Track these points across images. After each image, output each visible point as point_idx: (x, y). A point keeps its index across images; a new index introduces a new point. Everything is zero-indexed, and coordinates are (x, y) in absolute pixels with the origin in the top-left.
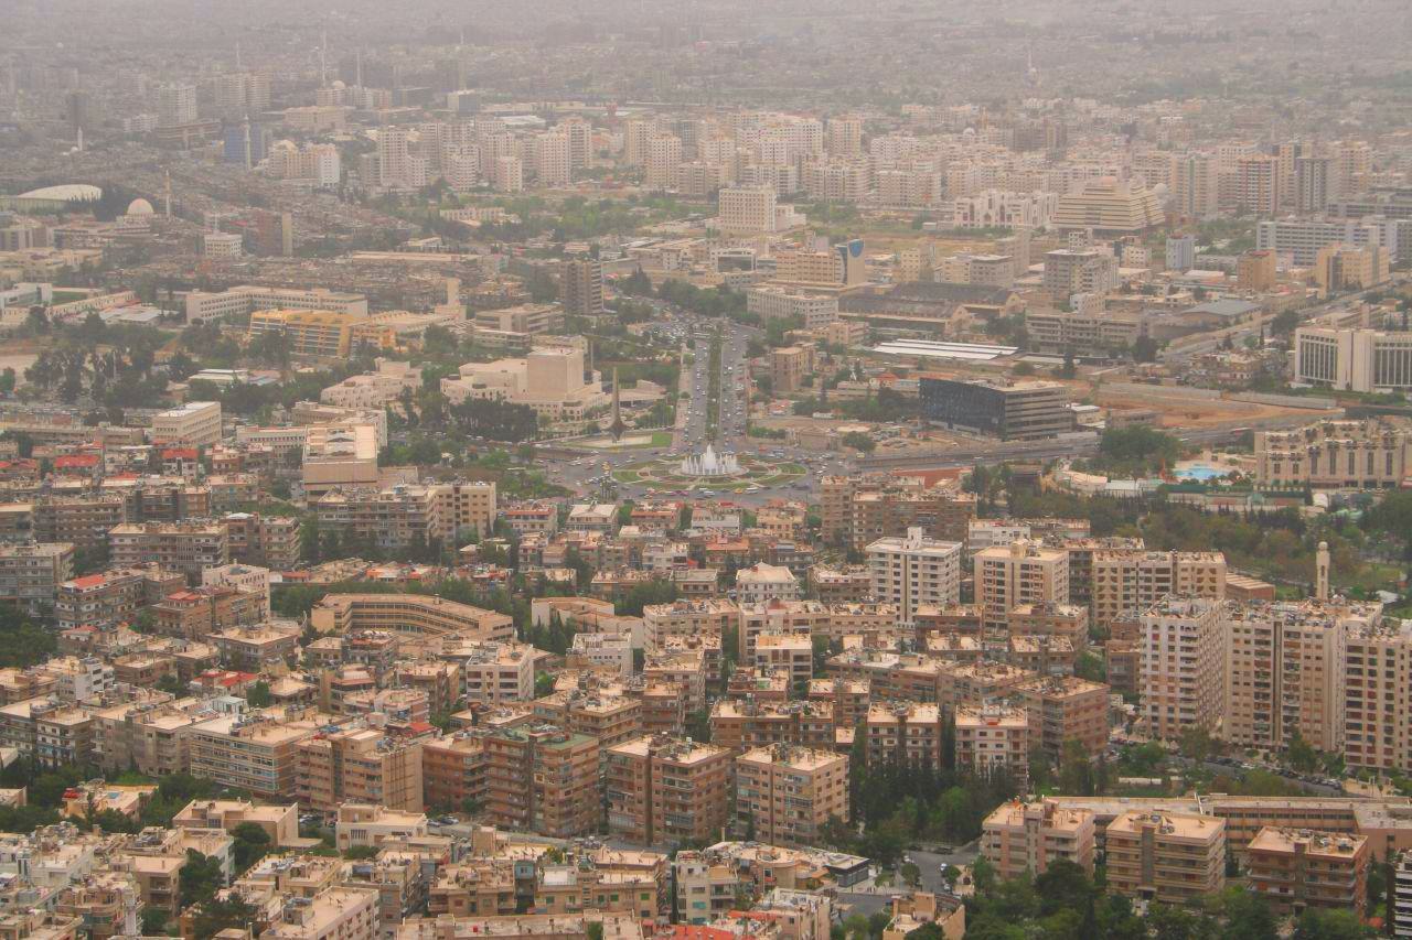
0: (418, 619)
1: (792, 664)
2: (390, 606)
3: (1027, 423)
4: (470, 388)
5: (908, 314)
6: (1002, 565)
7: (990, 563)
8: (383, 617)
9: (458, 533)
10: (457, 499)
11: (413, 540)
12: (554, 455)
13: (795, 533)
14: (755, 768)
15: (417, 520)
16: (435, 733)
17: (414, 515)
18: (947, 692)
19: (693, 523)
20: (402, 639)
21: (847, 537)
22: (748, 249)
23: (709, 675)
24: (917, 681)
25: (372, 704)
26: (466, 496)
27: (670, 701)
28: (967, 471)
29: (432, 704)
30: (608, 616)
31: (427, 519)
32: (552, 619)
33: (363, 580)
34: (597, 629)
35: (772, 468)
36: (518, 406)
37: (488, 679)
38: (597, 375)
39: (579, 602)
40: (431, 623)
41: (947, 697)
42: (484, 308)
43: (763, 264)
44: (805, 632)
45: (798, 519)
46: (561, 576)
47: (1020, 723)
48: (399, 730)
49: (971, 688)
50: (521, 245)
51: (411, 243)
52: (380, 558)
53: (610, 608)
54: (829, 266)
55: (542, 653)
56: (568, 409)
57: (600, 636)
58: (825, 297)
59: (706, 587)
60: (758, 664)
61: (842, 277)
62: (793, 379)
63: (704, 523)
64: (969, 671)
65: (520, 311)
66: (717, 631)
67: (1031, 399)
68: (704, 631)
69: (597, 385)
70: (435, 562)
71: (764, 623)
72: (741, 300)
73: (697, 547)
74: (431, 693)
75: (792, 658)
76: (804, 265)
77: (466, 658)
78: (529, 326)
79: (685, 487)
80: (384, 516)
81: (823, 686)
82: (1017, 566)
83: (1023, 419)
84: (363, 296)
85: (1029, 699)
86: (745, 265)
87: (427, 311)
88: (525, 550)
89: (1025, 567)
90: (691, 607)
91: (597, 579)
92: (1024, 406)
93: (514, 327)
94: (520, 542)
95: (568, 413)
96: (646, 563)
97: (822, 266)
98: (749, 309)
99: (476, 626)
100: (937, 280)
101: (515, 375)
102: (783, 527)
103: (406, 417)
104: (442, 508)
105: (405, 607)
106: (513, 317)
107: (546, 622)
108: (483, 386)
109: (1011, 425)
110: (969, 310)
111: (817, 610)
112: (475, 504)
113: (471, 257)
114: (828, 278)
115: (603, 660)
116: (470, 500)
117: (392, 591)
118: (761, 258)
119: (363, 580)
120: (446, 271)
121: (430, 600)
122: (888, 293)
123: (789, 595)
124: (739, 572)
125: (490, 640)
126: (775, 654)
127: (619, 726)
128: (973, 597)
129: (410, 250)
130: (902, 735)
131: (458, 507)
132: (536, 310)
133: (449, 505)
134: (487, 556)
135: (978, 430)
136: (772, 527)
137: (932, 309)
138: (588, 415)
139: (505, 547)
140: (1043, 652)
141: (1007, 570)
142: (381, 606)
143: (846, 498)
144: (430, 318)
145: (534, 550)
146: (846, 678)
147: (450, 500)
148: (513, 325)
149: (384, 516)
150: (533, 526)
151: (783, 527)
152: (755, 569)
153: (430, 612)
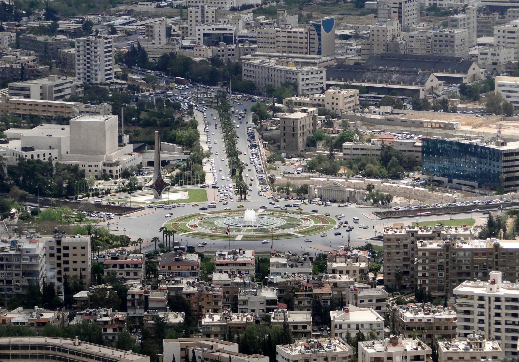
2: (33, 347)
4: (19, 150)
5: (387, 83)
26: (66, 248)
28: (482, 220)
35: (306, 219)
43: (243, 39)
45: (363, 265)
50: (17, 23)
53: (234, 347)
54: (304, 40)
56: (108, 169)
58: (314, 68)
59: (304, 327)
62: (300, 140)
65: (45, 81)
72: (237, 70)
76: (281, 44)
78: (55, 95)
79: (234, 237)
82: (493, 299)
88: (133, 295)
90: (320, 346)
91: (206, 320)
93: (43, 96)
95: (108, 172)
97: (299, 40)
98: (244, 78)
100: (402, 52)
101: (59, 139)
106: (41, 88)
108: (32, 149)
110: (439, 78)
112: (75, 255)
114: (298, 50)
116: (70, 251)
131: (59, 258)
132: (60, 81)
135: (476, 184)
137: (407, 78)
142: (25, 347)
143: (405, 246)
145: (140, 295)
148: (41, 94)
150: (128, 274)
153: (72, 353)
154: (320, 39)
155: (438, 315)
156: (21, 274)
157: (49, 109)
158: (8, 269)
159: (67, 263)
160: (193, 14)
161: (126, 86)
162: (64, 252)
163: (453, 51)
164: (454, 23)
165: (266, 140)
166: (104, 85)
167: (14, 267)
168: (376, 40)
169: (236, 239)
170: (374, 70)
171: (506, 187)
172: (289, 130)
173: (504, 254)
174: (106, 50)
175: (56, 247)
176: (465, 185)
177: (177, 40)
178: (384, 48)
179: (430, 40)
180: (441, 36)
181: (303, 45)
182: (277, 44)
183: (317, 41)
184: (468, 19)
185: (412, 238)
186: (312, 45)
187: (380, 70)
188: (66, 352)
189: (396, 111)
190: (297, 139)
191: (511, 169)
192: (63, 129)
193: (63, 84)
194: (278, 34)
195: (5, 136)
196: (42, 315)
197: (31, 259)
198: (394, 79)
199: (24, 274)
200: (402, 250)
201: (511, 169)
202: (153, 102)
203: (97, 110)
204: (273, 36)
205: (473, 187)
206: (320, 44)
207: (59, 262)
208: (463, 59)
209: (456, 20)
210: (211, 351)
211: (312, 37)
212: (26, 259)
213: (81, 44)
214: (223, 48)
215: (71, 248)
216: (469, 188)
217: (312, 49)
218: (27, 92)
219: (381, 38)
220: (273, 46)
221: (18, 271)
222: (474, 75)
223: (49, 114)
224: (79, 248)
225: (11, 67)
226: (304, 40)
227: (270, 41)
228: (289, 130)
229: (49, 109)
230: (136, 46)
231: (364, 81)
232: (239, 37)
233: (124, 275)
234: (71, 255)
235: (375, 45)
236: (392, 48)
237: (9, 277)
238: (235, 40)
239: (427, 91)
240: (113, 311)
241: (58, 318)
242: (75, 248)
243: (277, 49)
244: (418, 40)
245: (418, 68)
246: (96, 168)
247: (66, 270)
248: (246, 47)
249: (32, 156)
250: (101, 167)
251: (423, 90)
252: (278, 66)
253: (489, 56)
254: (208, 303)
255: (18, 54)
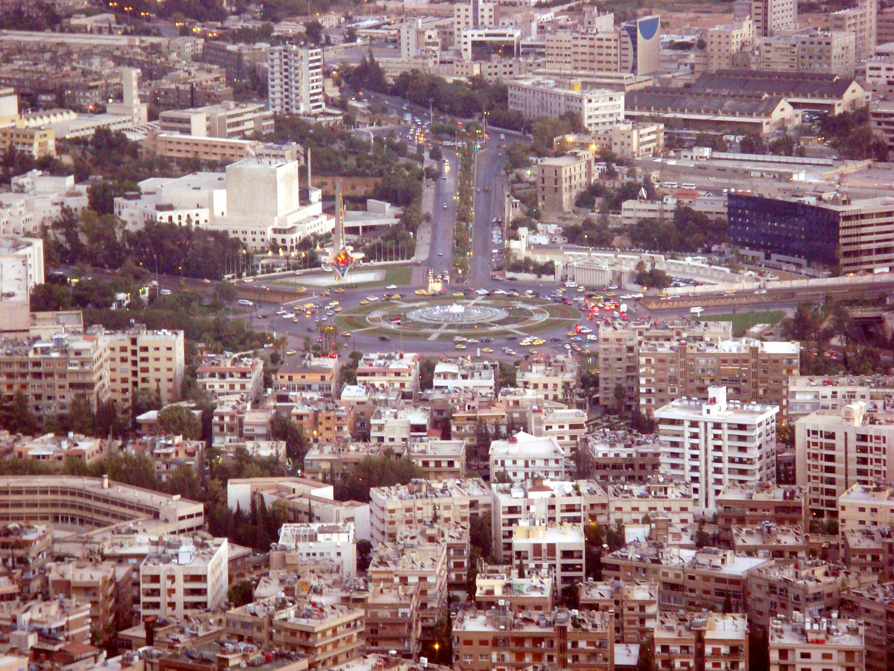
0: (81, 508)
1: (559, 561)
2: (44, 491)
3: (869, 252)
6: (832, 436)
7: (815, 433)
8: (35, 505)
9: (134, 398)
10: (134, 353)
11: (75, 404)
12: (261, 296)
13: (565, 394)
14: (69, 95)
15: (80, 379)
16: (96, 658)
17: (77, 373)
18: (760, 600)
19: (437, 382)
20: (59, 534)
21: (631, 399)
22: (509, 31)
23: (453, 576)
24: (722, 586)
25: (14, 620)
26: (145, 349)
27: (401, 610)
29: (94, 618)
30: (325, 501)
31: (95, 378)
32: (253, 503)
33: (8, 458)
34: (311, 517)
36: (215, 234)
37: (169, 585)
38: (316, 195)
39: (286, 482)
40: (98, 512)
41: (759, 607)
42: (168, 107)
44: (576, 520)
46: (265, 450)
47: (854, 643)
48: (49, 654)
49: (791, 596)
50: (219, 24)
51: (74, 21)
52: (33, 430)
53: (328, 492)
54: (613, 51)
55: (240, 550)
56: (279, 237)
57: (315, 526)
59: (451, 464)
60: (516, 562)
61: (630, 65)
62: (566, 197)
63: (450, 383)
64: (788, 573)
65: (218, 111)
66: (464, 519)
67: (875, 220)
68: (447, 520)
69: (316, 207)
70: (103, 435)
71: (524, 509)
73: (440, 412)
74: (94, 604)
75: (558, 554)
76: (580, 57)
77: (141, 557)
78: (229, 130)
80: (38, 375)
81: (598, 591)
83: (863, 247)
84: (11, 90)
85: (867, 611)
86: (508, 50)
87: (101, 110)
89: (863, 438)
91: (313, 454)
92: (864, 230)
93: (210, 130)
94: (214, 407)
95: (279, 242)
96: (374, 434)
97: (605, 51)
98: (511, 107)
99: (156, 515)
100: (754, 67)
102: (550, 387)
103: (68, 246)
104: (114, 365)
105: (64, 492)
107: (246, 507)
108: (170, 207)
109: (847, 254)
111: (592, 492)
112: (157, 359)
113: (155, 40)
114: (604, 66)
115: (318, 557)
116: (151, 354)
117: (47, 472)
118: (528, 41)
119: (8, 458)
120: (122, 60)
121: (96, 482)
122: (687, 86)
123: (557, 473)
124: (494, 444)
125: (173, 533)
126: (537, 548)
127: (335, 644)
128: (794, 475)
129: (73, 30)
130: (700, 654)
131: (134, 363)
133: (124, 360)
134: (167, 425)
136: (536, 386)
137: (745, 105)
138: (305, 244)
139: (197, 413)
140: (886, 548)
141: (839, 442)
142: (32, 491)
143: (630, 349)
144: (101, 121)
146: (629, 580)
147: (124, 354)
148: (208, 129)
149: (38, 375)
151: (550, 387)
152: (514, 441)
153: (97, 499)
154: (635, 49)
155: (643, 449)
156: (67, 386)
157: (214, 150)
158: (49, 379)
159: (145, 370)
160: (463, 13)
161: (341, 118)
162: (141, 354)
163: (829, 65)
164: (839, 23)
165: (517, 198)
166: (309, 116)
167: (56, 377)
168: (716, 50)
169: (430, 339)
170: (699, 94)
171: (847, 265)
172: (550, 183)
173: (765, 361)
174: (311, 65)
175: (130, 347)
176: (788, 263)
177: (434, 51)
178: (727, 61)
179: (795, 49)
180: (812, 43)
181: (612, 58)
182: (574, 57)
183: (630, 52)
184: (861, 16)
185: (640, 338)
186: (624, 58)
187: (708, 95)
188: (89, 497)
189: (716, 155)
190: (561, 195)
191: (855, 239)
192: (220, 179)
193: (242, 114)
194: (575, 42)
195: (138, 189)
196: (76, 445)
197: (82, 364)
198: (726, 108)
199: (72, 386)
200: (624, 355)
201: (855, 239)
202: (369, 141)
203: (281, 153)
204: (568, 45)
205: (799, 266)
206: (635, 56)
207: (134, 368)
208: (837, 78)
209: (842, 19)
210: (292, 495)
211: (624, 46)
212: (75, 365)
213: (277, 55)
214: (495, 63)
215: (151, 349)
216: (794, 268)
217: (624, 65)
218: (186, 126)
219: (723, 47)
220: (568, 59)
221: (62, 382)
222: (854, 101)
223: (214, 158)
224: (163, 349)
225: (177, 88)
226: (613, 51)
227: (564, 52)
228: (550, 183)
229: (214, 150)
230: (368, 59)
231: (682, 111)
232: (523, 46)
233: (227, 388)
234: (151, 360)
235: (715, 57)
236: (739, 61)
237: (50, 392)
238: (518, 51)
239: (775, 124)
240: (185, 438)
241: (101, 448)
242: (158, 349)
243: (573, 64)
244: (777, 49)
245: (763, 90)
246: (263, 236)
247: (144, 380)
248: (530, 60)
249: (170, 218)
250: (270, 235)
251: (767, 123)
252: (556, 90)
253: (883, 73)
254: (327, 429)
255: (192, 70)
